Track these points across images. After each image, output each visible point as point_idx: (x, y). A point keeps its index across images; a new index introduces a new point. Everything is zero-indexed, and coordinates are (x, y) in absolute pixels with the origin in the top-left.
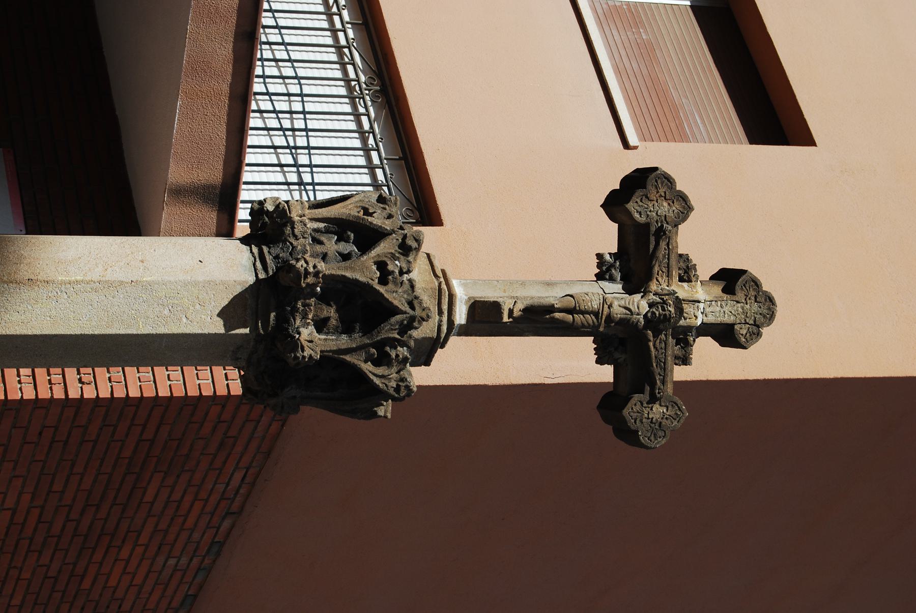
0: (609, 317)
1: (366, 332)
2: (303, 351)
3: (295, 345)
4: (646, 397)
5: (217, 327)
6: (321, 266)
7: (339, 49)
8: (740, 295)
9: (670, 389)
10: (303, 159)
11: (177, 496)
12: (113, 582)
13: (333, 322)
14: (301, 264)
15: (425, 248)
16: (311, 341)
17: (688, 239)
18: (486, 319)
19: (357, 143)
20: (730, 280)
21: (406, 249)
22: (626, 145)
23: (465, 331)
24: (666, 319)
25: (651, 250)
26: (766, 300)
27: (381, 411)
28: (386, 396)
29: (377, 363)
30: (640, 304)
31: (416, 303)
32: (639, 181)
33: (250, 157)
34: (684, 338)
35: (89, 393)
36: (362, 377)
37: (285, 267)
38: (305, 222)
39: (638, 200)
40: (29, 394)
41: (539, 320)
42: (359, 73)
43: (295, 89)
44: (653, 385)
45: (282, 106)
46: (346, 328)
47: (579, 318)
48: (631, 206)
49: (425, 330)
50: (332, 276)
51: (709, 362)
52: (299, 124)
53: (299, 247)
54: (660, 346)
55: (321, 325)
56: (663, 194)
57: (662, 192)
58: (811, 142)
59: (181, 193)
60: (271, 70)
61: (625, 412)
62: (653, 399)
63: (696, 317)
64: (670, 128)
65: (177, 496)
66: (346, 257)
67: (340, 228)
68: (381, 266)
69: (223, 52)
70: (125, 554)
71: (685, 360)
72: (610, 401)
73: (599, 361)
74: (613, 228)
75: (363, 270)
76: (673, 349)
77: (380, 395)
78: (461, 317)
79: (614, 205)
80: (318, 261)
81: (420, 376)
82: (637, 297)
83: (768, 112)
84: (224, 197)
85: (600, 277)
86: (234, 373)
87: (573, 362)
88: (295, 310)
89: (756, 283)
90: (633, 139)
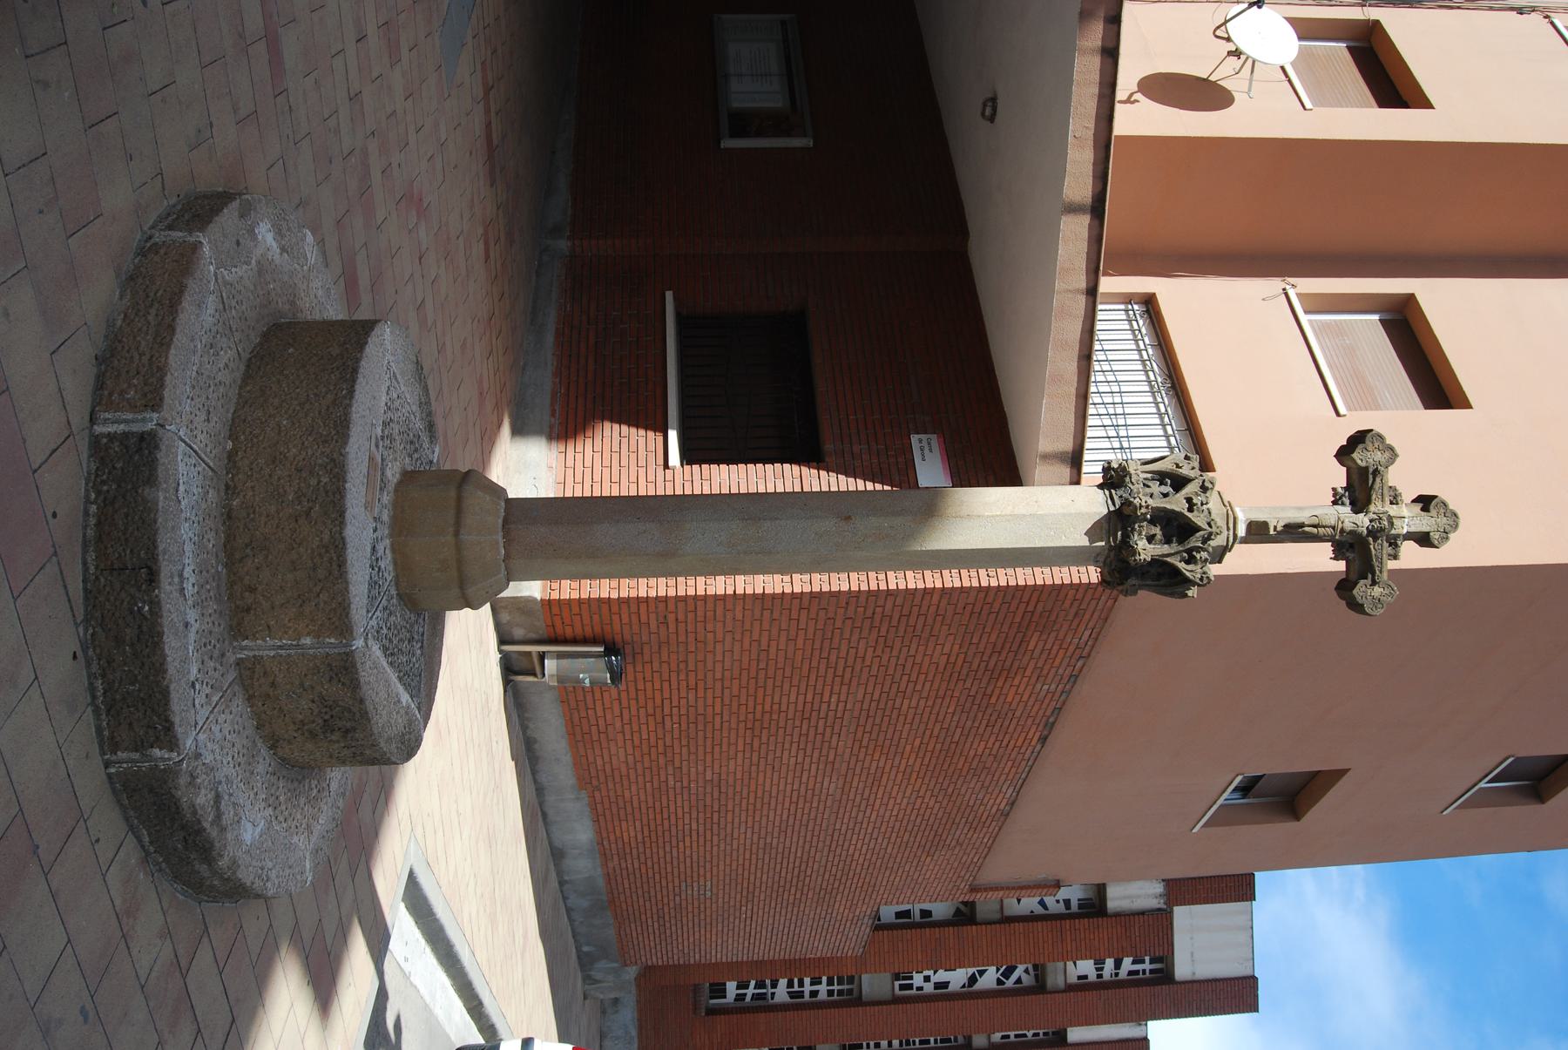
0: (1342, 530)
1: (1180, 542)
3: (1134, 552)
4: (1369, 581)
5: (1085, 542)
6: (1150, 502)
7: (1143, 361)
8: (1433, 512)
9: (1385, 575)
10: (1123, 433)
11: (1048, 646)
12: (1009, 699)
14: (1137, 501)
15: (1217, 488)
16: (1145, 549)
17: (1394, 476)
18: (1258, 532)
19: (1158, 421)
20: (1425, 502)
21: (1204, 489)
22: (666, 466)
23: (1245, 541)
24: (1382, 530)
27: (1190, 593)
28: (1193, 583)
29: (1188, 562)
30: (1363, 521)
32: (1358, 439)
33: (1089, 433)
34: (1394, 542)
35: (994, 583)
36: (1176, 572)
37: (1126, 503)
38: (1138, 474)
40: (957, 584)
41: (1294, 532)
42: (1157, 376)
43: (1116, 389)
44: (1373, 574)
45: (1108, 399)
46: (1168, 541)
47: (1321, 530)
48: (1355, 455)
49: (1218, 541)
50: (1158, 509)
51: (1412, 557)
52: (1119, 411)
54: (1378, 548)
55: (1150, 539)
58: (1469, 406)
59: (1046, 457)
60: (1100, 377)
61: (1355, 592)
62: (1374, 583)
63: (1403, 528)
64: (1373, 405)
65: (1048, 646)
66: (1165, 495)
67: (1161, 477)
68: (1189, 500)
69: (1072, 368)
70: (1016, 682)
71: (1395, 557)
72: (1345, 586)
73: (1336, 558)
74: (1342, 472)
75: (1177, 503)
76: (1387, 549)
77: (1188, 582)
78: (1241, 531)
79: (1343, 454)
80: (1149, 497)
81: (1214, 570)
82: (1361, 515)
83: (1436, 386)
84: (1075, 460)
85: (1335, 503)
86: (1092, 569)
87: (1319, 559)
88: (1133, 530)
89: (1445, 504)
90: (1342, 410)
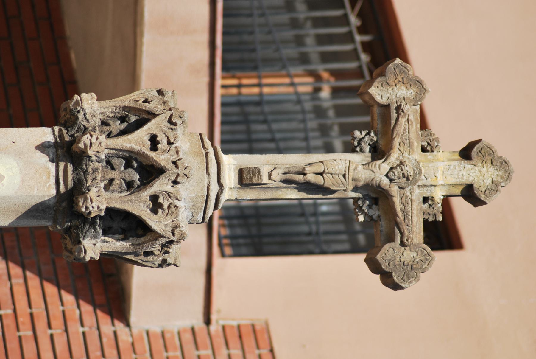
2: (91, 202)
13: (117, 182)
25: (392, 127)
26: (502, 163)
31: (179, 163)
39: (380, 85)
53: (90, 128)
56: (401, 80)
57: (400, 78)
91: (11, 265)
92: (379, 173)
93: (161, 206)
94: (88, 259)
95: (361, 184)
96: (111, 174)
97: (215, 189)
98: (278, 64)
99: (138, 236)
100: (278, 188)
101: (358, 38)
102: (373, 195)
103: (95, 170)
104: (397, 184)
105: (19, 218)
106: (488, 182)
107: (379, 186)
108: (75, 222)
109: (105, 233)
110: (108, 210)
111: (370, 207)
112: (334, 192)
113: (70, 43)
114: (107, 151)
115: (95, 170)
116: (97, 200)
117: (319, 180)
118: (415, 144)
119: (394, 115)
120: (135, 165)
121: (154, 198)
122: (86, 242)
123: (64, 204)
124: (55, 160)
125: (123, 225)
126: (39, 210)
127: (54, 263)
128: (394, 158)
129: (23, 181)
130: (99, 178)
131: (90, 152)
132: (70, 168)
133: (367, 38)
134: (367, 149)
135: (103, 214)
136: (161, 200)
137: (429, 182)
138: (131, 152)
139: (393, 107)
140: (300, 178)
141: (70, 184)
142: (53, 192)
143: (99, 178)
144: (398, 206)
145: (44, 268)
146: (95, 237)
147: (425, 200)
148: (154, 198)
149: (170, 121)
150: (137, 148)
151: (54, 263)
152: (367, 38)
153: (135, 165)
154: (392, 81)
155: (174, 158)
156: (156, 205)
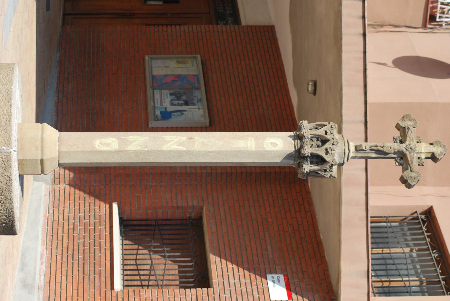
13: (314, 145)
91: (298, 296)
92: (402, 147)
93: (328, 152)
94: (305, 172)
95: (396, 151)
96: (312, 143)
97: (347, 151)
98: (397, 244)
99: (322, 164)
100: (368, 152)
101: (426, 234)
102: (401, 156)
103: (307, 142)
104: (409, 151)
105: (283, 159)
106: (439, 152)
107: (402, 152)
108: (301, 160)
109: (311, 164)
110: (311, 154)
111: (400, 160)
112: (388, 154)
113: (320, 232)
114: (310, 135)
115: (307, 142)
116: (307, 150)
117: (382, 149)
118: (414, 140)
119: (407, 130)
120: (320, 140)
121: (326, 150)
122: (305, 166)
123: (297, 154)
124: (294, 140)
125: (317, 160)
126: (289, 156)
127: (313, 296)
128: (407, 143)
129: (284, 146)
130: (308, 144)
131: (305, 135)
132: (299, 141)
133: (429, 234)
134: (399, 141)
135: (310, 155)
136: (328, 150)
137: (420, 151)
138: (318, 135)
139: (406, 128)
140: (375, 148)
141: (299, 147)
142: (294, 150)
143: (308, 144)
144: (409, 159)
145: (310, 297)
146: (307, 164)
147: (419, 158)
148: (326, 150)
149: (331, 127)
150: (320, 134)
151: (313, 296)
152: (429, 234)
153: (320, 140)
154: (406, 119)
155: (333, 137)
156: (327, 153)
